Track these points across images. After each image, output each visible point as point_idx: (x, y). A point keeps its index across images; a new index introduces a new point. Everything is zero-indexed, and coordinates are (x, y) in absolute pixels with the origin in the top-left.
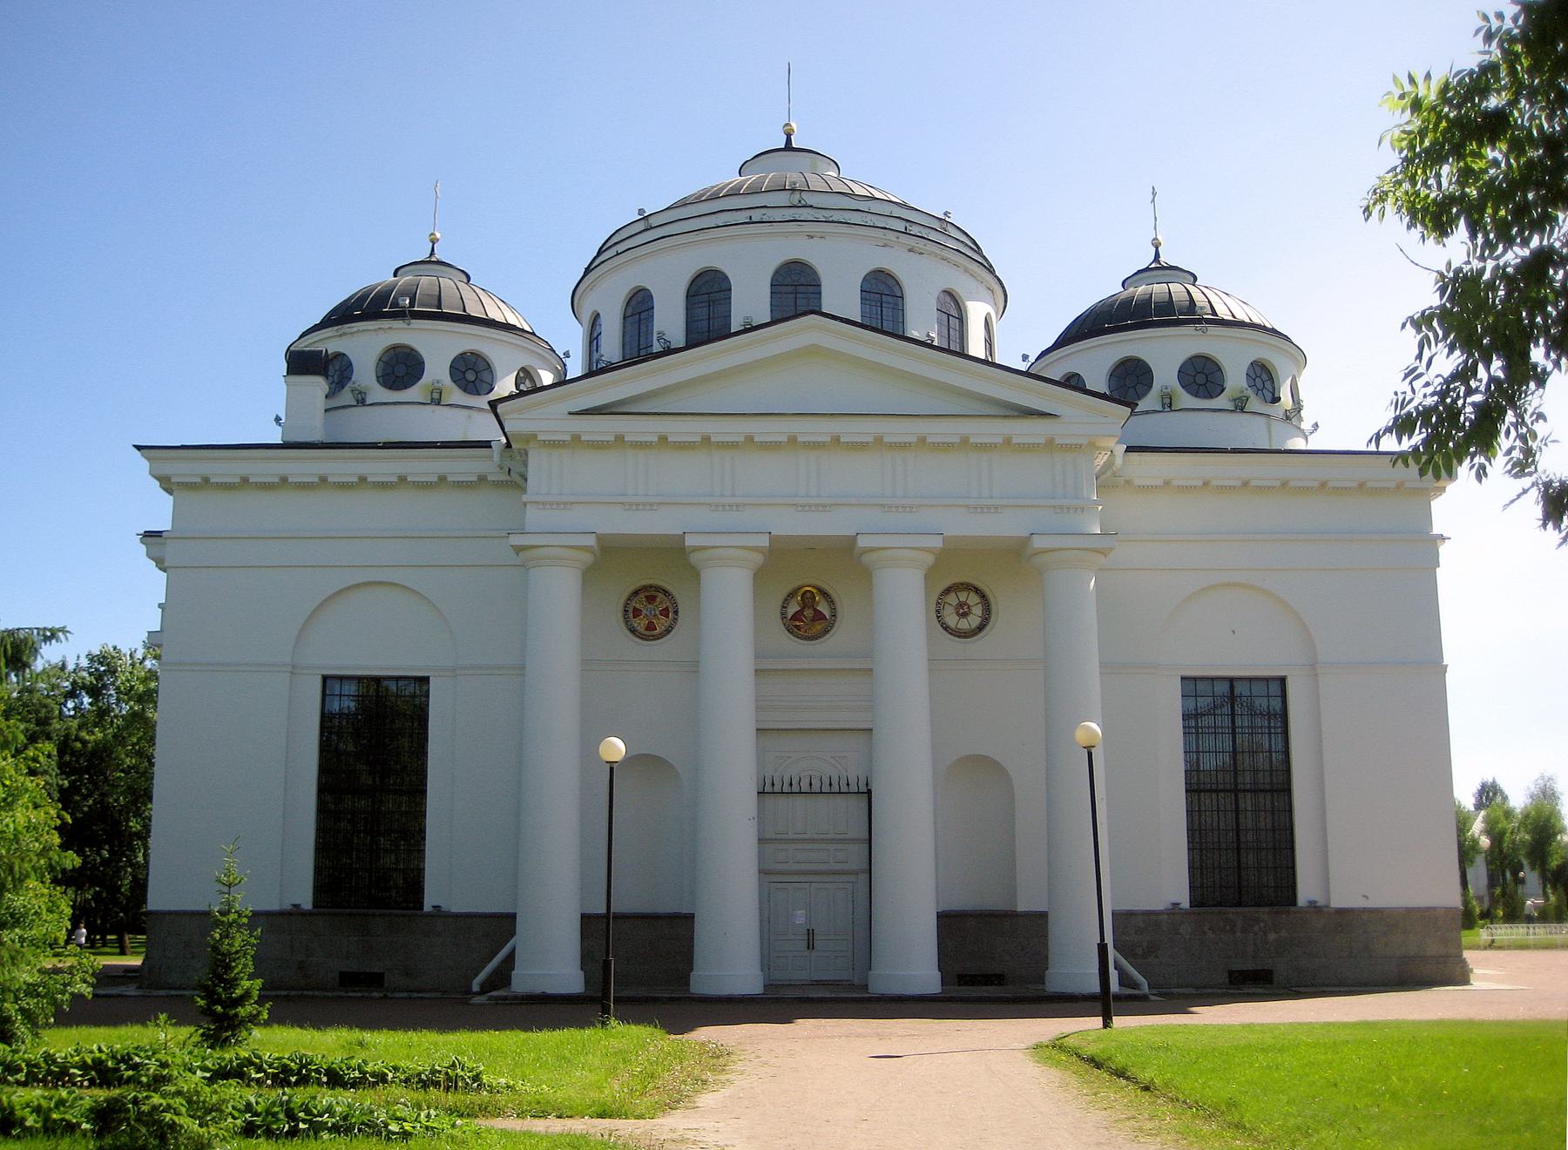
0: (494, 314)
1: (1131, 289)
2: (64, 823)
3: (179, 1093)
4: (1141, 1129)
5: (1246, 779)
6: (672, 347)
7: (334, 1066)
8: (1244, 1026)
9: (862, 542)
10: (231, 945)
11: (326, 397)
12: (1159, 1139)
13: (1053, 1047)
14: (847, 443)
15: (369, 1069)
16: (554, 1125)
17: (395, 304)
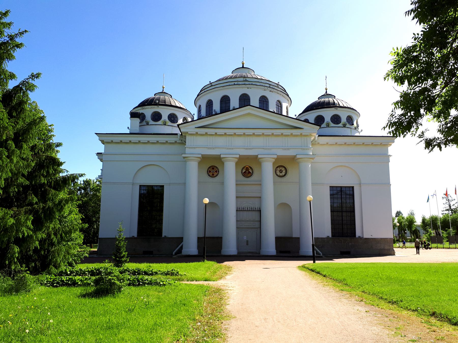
0: (178, 105)
1: (320, 100)
2: (83, 218)
3: (115, 276)
4: (324, 284)
5: (344, 209)
6: (217, 113)
7: (146, 271)
8: (345, 263)
9: (259, 156)
10: (121, 245)
11: (140, 123)
12: (329, 287)
13: (302, 267)
14: (256, 135)
15: (153, 271)
16: (194, 283)
17: (155, 102)
